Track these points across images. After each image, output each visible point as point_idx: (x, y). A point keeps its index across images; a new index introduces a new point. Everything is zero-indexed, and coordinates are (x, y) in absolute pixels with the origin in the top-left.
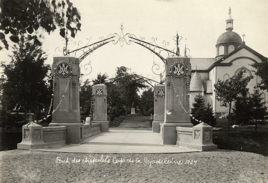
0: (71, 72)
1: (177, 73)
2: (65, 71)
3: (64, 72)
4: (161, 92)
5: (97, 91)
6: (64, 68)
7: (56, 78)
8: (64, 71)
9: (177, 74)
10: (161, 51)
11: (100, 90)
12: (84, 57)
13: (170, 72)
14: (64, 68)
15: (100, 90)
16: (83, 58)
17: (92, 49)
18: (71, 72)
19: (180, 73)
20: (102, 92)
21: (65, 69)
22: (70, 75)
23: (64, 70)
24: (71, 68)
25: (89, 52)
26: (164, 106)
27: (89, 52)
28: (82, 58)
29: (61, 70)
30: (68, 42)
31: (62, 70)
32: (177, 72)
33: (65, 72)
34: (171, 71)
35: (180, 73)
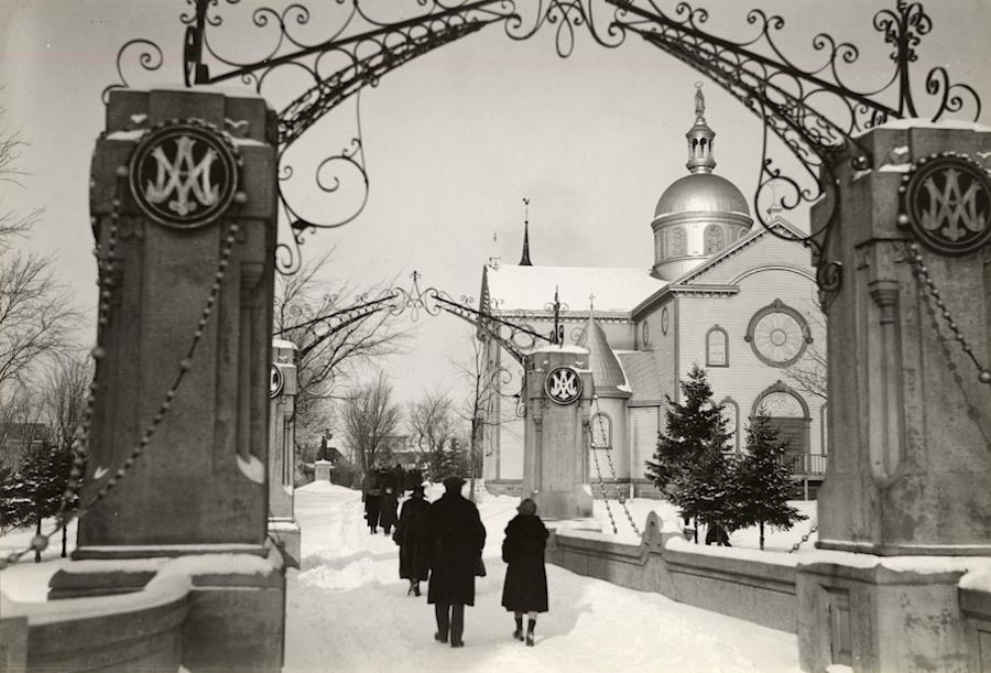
0: (241, 197)
1: (946, 223)
2: (966, 220)
3: (954, 218)
4: (561, 383)
5: (553, 380)
6: (184, 167)
7: (126, 234)
8: (956, 216)
9: (945, 231)
10: (769, 75)
11: (568, 376)
12: (315, 108)
13: (122, 170)
14: (953, 197)
15: (568, 376)
16: (308, 118)
17: (373, 63)
18: (241, 197)
19: (961, 224)
20: (576, 383)
21: (194, 173)
22: (223, 221)
23: (953, 208)
24: (239, 168)
25: (352, 81)
26: (228, 585)
27: (352, 81)
28: (302, 115)
29: (167, 177)
30: (911, 66)
31: (945, 211)
32: (941, 217)
33: (960, 218)
34: (127, 164)
35: (961, 224)
